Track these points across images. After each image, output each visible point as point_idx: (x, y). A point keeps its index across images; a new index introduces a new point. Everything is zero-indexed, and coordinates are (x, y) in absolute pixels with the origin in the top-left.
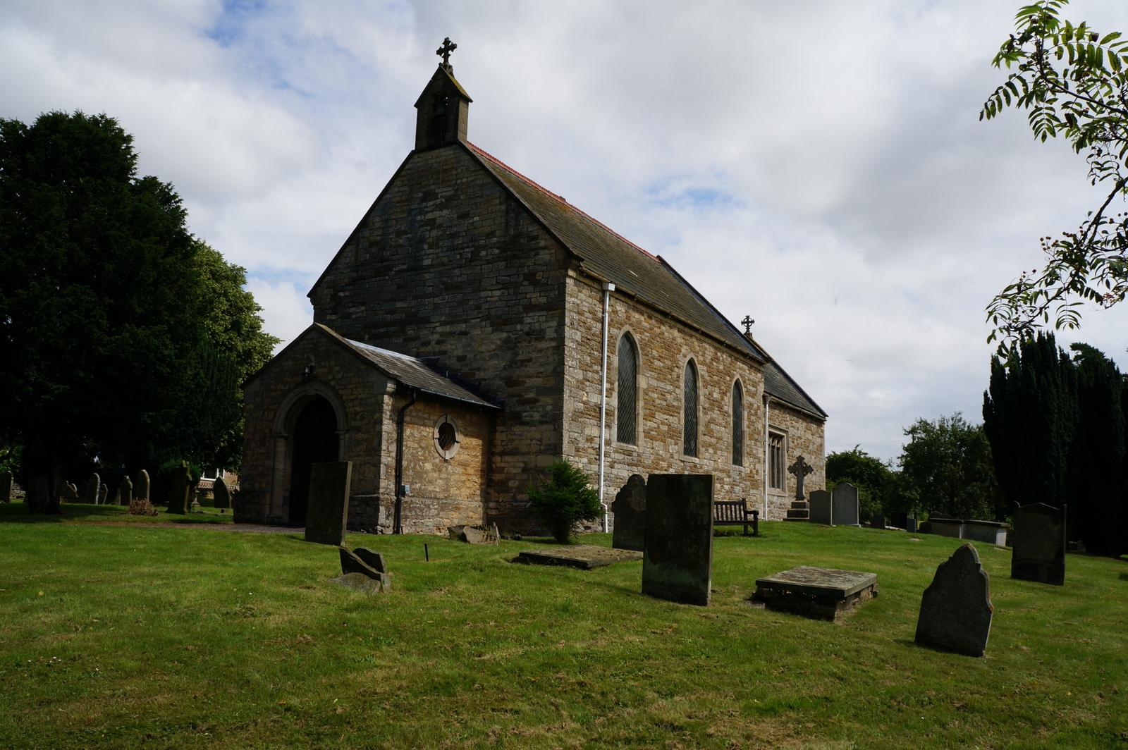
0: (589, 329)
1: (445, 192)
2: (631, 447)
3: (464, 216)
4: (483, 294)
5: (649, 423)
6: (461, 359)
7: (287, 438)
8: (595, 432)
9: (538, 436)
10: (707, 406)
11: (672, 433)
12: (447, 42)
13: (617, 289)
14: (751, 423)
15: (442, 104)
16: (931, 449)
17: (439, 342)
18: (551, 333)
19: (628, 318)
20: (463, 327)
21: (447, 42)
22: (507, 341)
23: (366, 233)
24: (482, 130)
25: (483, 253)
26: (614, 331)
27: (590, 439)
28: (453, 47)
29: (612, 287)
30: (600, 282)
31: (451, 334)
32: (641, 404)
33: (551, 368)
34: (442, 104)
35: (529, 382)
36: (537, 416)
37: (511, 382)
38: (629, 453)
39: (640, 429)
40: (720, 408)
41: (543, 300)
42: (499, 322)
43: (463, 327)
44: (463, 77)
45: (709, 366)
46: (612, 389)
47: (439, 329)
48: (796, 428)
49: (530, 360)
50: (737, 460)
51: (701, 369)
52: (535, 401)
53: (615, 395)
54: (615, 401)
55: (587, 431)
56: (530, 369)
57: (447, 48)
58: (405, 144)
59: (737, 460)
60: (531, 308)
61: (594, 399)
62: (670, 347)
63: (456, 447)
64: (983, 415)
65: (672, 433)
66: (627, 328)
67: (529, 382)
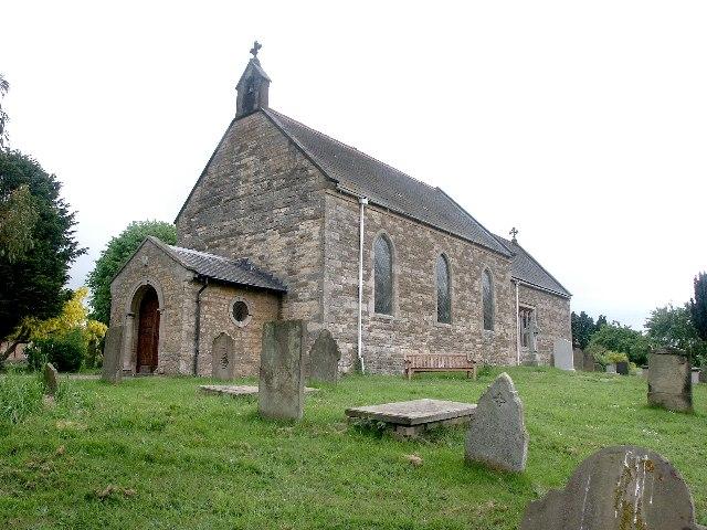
0: (347, 231)
1: (252, 144)
2: (388, 316)
3: (264, 159)
4: (275, 211)
5: (404, 300)
6: (261, 258)
7: (134, 316)
8: (354, 306)
9: (308, 309)
10: (459, 286)
11: (428, 307)
12: (256, 44)
13: (370, 203)
14: (500, 300)
15: (252, 91)
16: (664, 324)
17: (248, 247)
18: (316, 235)
19: (384, 223)
20: (262, 236)
21: (256, 44)
22: (289, 243)
23: (206, 178)
24: (280, 101)
25: (275, 183)
26: (370, 233)
27: (349, 311)
28: (260, 47)
29: (365, 201)
30: (356, 198)
31: (255, 241)
32: (396, 285)
33: (315, 260)
34: (252, 91)
35: (303, 271)
36: (307, 295)
37: (291, 272)
38: (387, 321)
39: (396, 304)
40: (471, 289)
41: (311, 212)
42: (286, 230)
43: (262, 236)
44: (267, 67)
45: (460, 259)
46: (369, 275)
47: (249, 238)
48: (542, 305)
49: (303, 255)
50: (488, 325)
51: (453, 262)
52: (306, 284)
53: (372, 278)
54: (372, 283)
55: (347, 305)
56: (303, 262)
57: (257, 47)
58: (230, 111)
59: (488, 325)
60: (303, 218)
61: (353, 282)
62: (425, 247)
63: (249, 319)
64: (422, 184)
65: (428, 307)
66: (383, 231)
67: (303, 271)
